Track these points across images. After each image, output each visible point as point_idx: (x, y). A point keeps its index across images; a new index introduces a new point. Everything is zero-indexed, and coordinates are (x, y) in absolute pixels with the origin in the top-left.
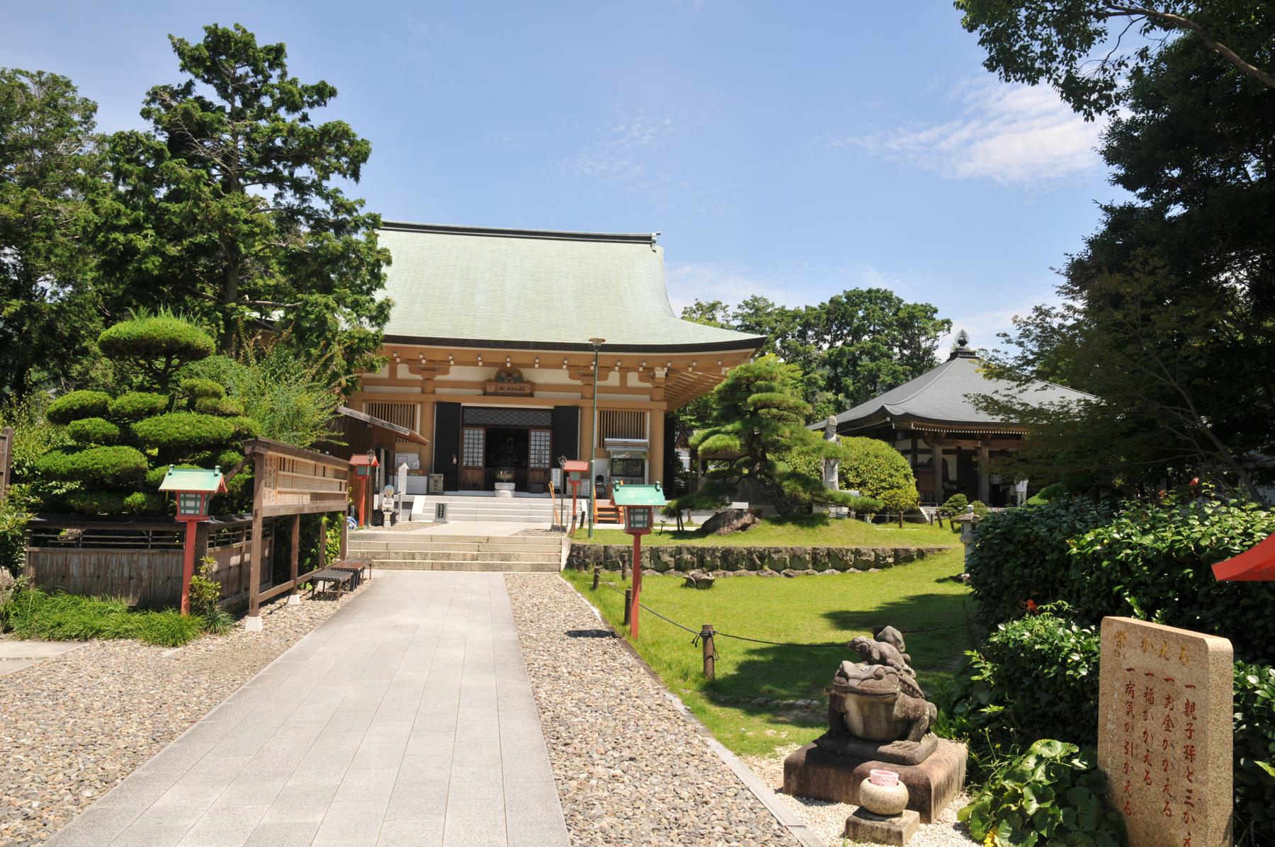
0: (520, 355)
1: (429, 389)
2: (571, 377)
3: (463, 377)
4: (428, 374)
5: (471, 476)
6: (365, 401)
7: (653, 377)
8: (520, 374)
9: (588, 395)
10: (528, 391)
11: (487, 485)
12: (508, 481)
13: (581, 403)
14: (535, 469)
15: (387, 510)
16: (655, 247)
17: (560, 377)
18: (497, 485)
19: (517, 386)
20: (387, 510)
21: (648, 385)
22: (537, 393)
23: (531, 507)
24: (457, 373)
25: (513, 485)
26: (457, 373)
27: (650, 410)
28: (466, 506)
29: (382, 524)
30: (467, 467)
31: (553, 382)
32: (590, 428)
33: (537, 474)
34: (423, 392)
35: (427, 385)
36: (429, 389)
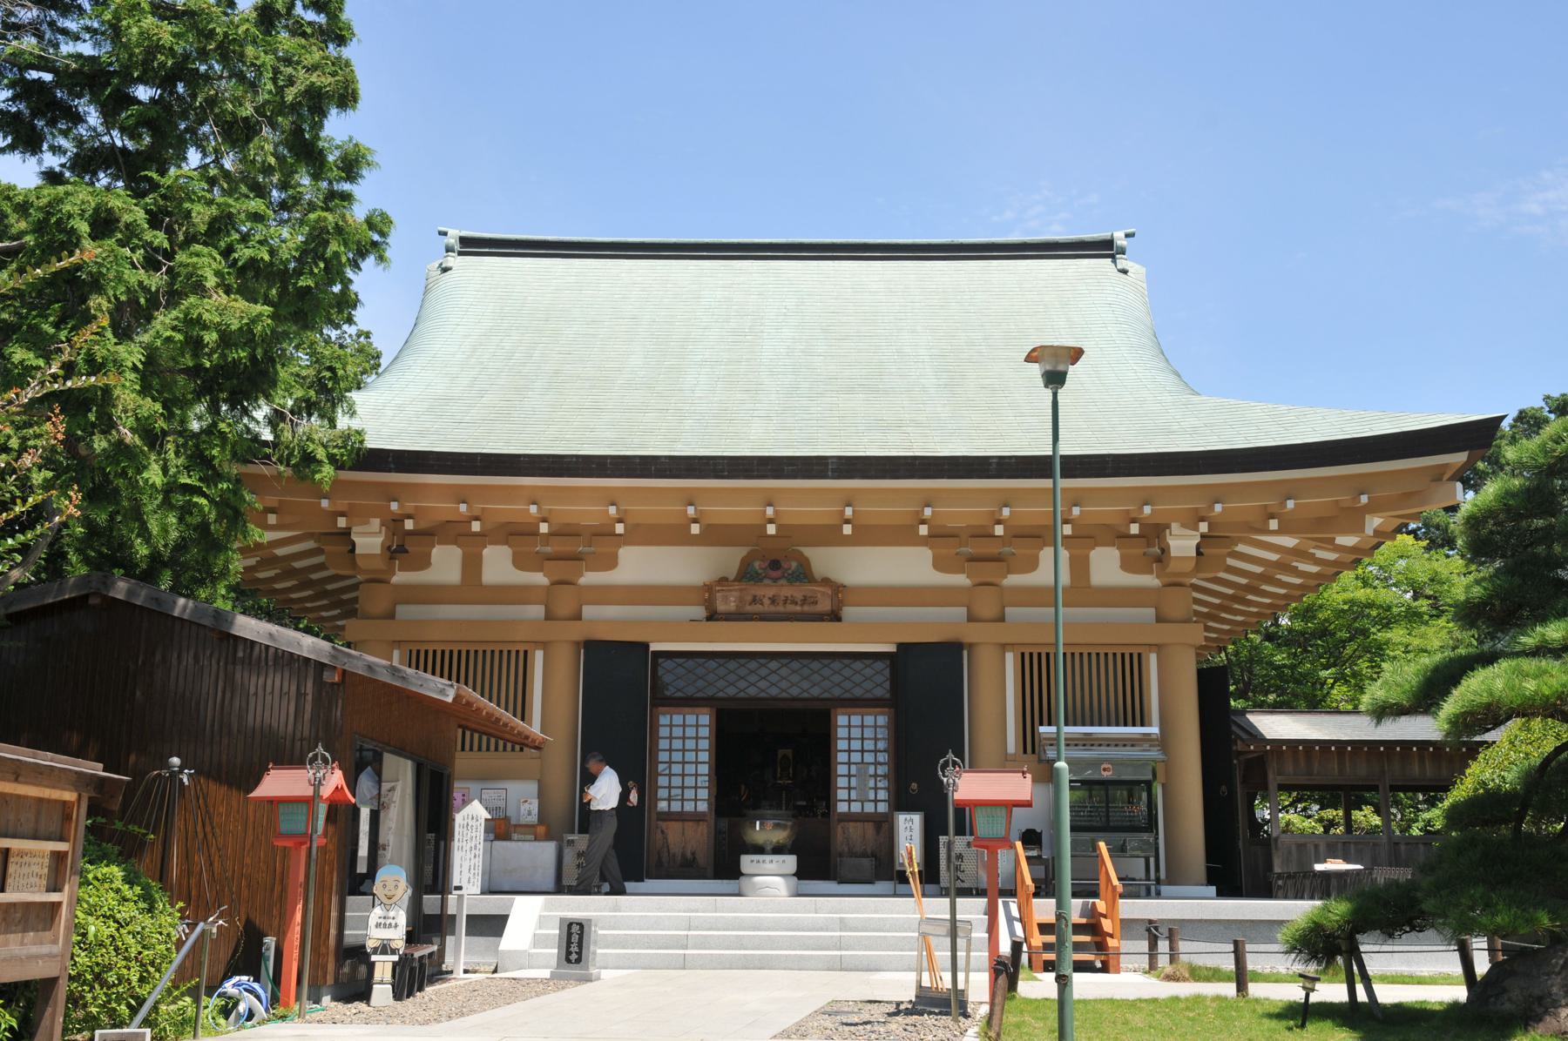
0: (804, 501)
1: (564, 609)
2: (939, 565)
3: (653, 582)
4: (562, 569)
5: (678, 838)
6: (398, 643)
7: (1163, 557)
8: (805, 563)
9: (988, 610)
10: (824, 606)
11: (722, 865)
12: (778, 850)
13: (970, 633)
14: (849, 817)
15: (385, 949)
16: (1123, 262)
17: (911, 566)
18: (747, 862)
19: (796, 591)
20: (385, 949)
21: (1150, 580)
22: (849, 612)
23: (843, 925)
24: (637, 565)
25: (790, 862)
26: (637, 565)
27: (1158, 647)
28: (657, 924)
29: (364, 994)
30: (669, 816)
31: (891, 581)
32: (995, 695)
33: (854, 830)
34: (549, 616)
35: (561, 600)
36: (564, 607)
